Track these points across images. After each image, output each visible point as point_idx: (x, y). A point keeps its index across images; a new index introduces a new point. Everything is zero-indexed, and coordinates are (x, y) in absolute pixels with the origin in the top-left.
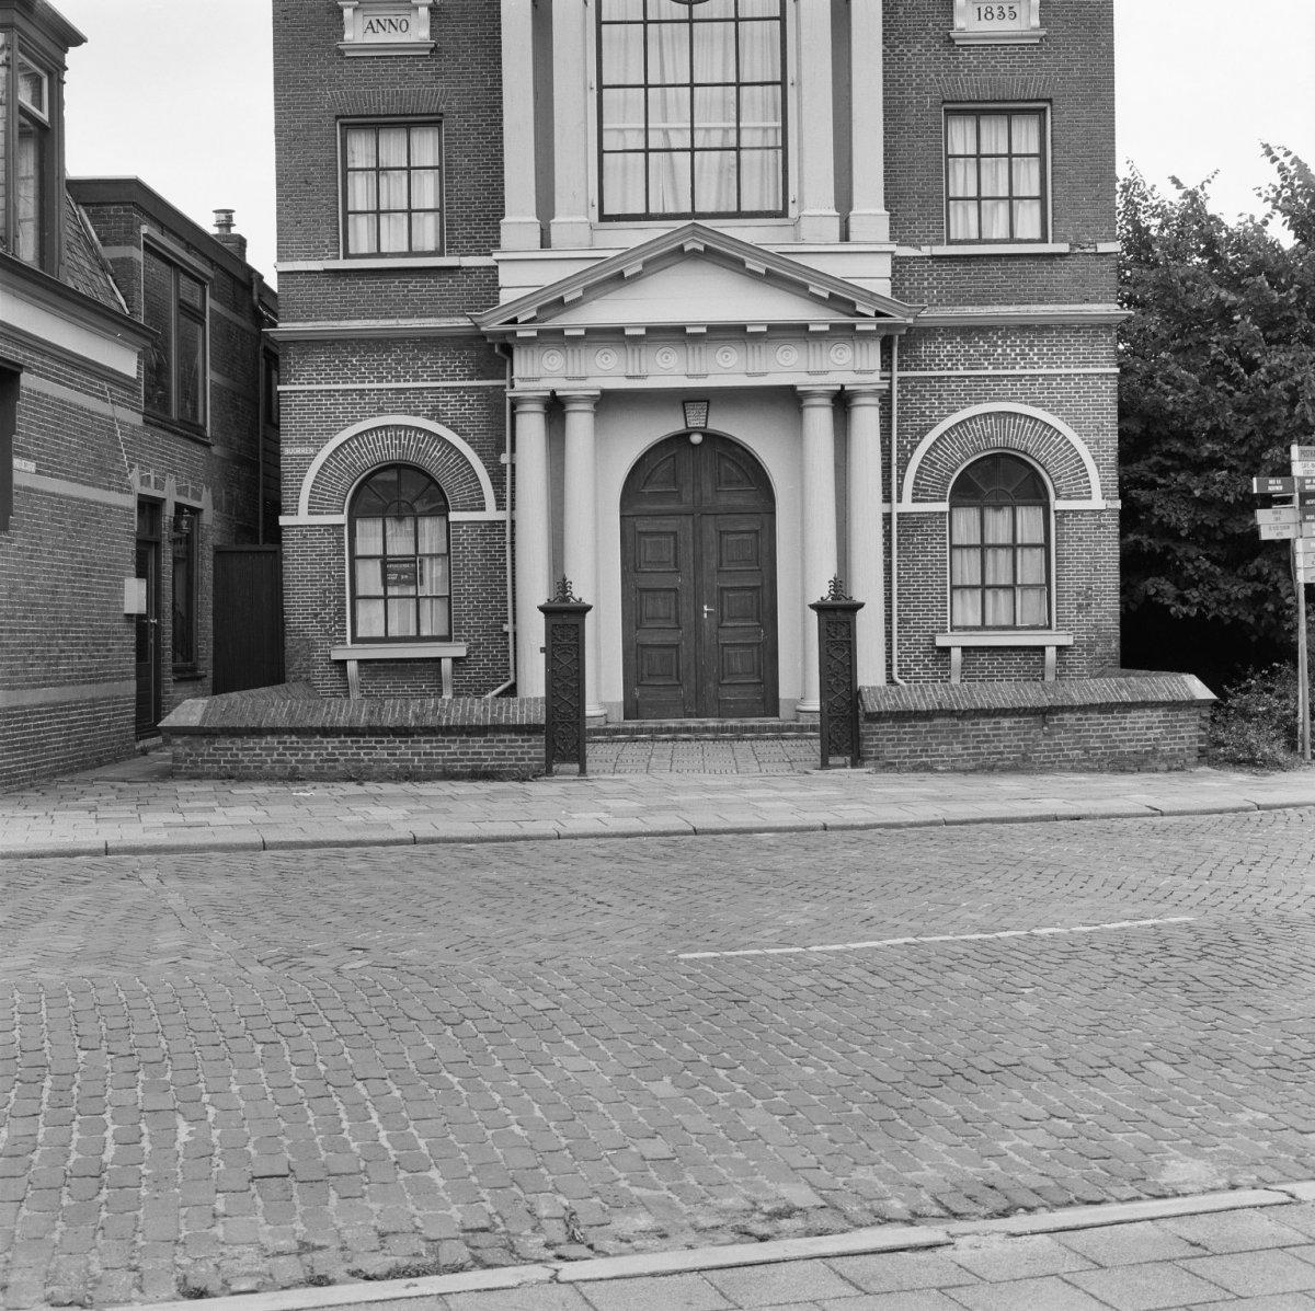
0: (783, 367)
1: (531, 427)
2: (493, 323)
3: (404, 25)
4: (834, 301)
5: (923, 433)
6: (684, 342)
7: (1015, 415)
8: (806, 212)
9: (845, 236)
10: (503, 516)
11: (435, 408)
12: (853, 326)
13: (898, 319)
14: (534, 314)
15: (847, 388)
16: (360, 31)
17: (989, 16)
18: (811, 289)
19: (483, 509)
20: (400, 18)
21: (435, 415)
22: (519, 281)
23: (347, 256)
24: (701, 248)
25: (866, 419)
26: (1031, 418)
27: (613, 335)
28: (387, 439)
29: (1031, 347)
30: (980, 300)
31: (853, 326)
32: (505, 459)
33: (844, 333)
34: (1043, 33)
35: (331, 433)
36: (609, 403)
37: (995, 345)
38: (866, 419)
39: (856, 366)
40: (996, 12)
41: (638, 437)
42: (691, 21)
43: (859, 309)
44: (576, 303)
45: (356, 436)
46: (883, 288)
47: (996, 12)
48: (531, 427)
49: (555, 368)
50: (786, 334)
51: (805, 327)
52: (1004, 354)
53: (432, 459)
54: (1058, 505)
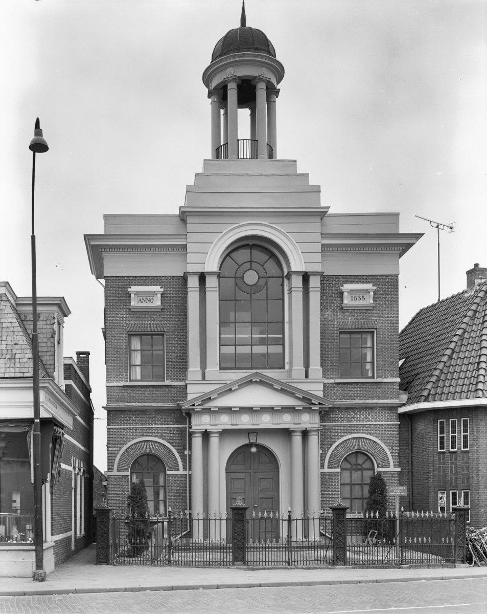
0: (286, 421)
1: (197, 442)
2: (186, 406)
3: (152, 300)
4: (304, 399)
5: (331, 445)
6: (251, 413)
7: (363, 438)
8: (294, 368)
9: (307, 376)
10: (186, 472)
11: (162, 435)
12: (310, 408)
13: (326, 405)
14: (200, 403)
15: (208, 430)
16: (137, 301)
17: (355, 299)
18: (296, 395)
19: (178, 470)
20: (151, 298)
21: (162, 437)
22: (194, 392)
23: (130, 381)
24: (259, 380)
25: (314, 440)
26: (369, 439)
27: (228, 410)
28: (144, 445)
29: (369, 414)
30: (351, 398)
31: (310, 408)
32: (186, 452)
33: (308, 410)
34: (374, 305)
35: (125, 443)
36: (225, 434)
37: (357, 414)
38: (314, 440)
39: (309, 421)
40: (358, 298)
41: (232, 446)
42: (251, 300)
43: (312, 402)
44: (214, 399)
45: (134, 444)
46: (321, 394)
47: (358, 298)
48: (197, 442)
49: (306, 420)
50: (286, 410)
51: (294, 408)
52: (360, 417)
53: (160, 453)
54: (168, 473)
